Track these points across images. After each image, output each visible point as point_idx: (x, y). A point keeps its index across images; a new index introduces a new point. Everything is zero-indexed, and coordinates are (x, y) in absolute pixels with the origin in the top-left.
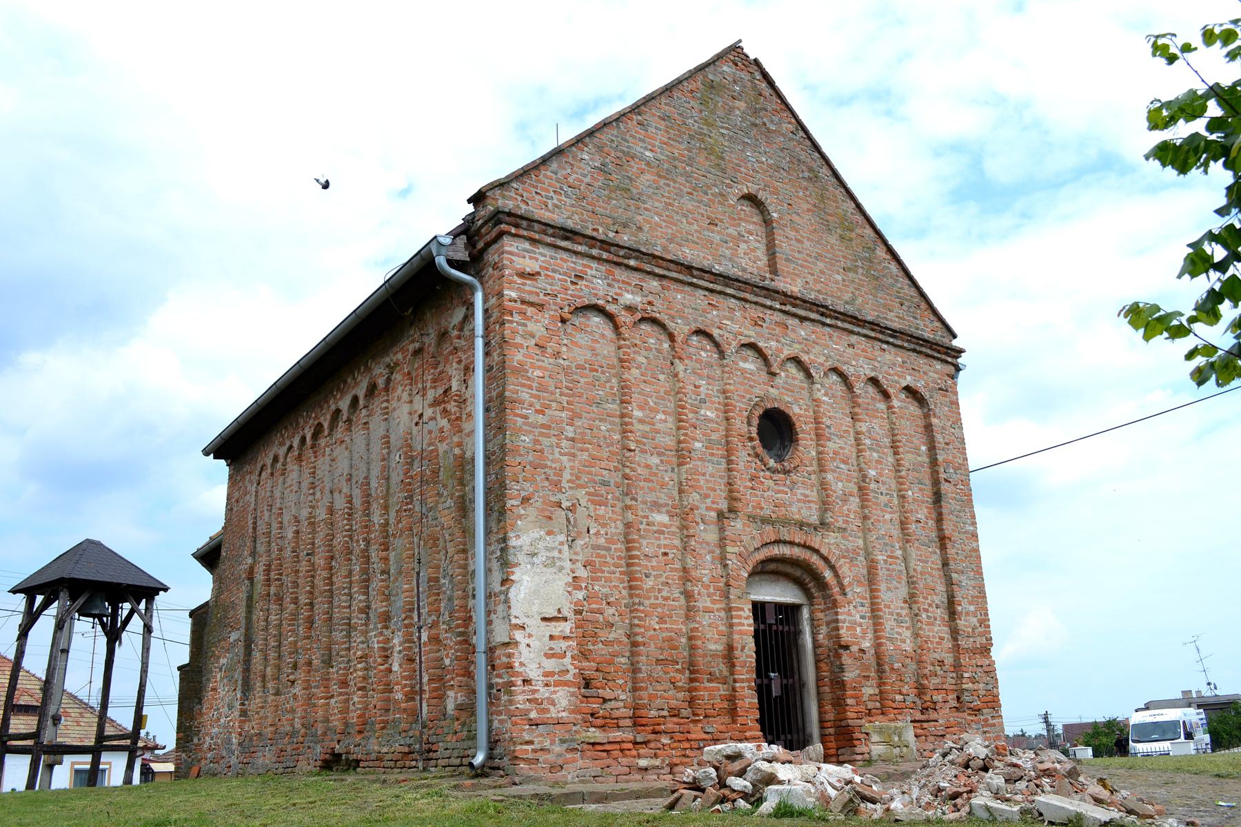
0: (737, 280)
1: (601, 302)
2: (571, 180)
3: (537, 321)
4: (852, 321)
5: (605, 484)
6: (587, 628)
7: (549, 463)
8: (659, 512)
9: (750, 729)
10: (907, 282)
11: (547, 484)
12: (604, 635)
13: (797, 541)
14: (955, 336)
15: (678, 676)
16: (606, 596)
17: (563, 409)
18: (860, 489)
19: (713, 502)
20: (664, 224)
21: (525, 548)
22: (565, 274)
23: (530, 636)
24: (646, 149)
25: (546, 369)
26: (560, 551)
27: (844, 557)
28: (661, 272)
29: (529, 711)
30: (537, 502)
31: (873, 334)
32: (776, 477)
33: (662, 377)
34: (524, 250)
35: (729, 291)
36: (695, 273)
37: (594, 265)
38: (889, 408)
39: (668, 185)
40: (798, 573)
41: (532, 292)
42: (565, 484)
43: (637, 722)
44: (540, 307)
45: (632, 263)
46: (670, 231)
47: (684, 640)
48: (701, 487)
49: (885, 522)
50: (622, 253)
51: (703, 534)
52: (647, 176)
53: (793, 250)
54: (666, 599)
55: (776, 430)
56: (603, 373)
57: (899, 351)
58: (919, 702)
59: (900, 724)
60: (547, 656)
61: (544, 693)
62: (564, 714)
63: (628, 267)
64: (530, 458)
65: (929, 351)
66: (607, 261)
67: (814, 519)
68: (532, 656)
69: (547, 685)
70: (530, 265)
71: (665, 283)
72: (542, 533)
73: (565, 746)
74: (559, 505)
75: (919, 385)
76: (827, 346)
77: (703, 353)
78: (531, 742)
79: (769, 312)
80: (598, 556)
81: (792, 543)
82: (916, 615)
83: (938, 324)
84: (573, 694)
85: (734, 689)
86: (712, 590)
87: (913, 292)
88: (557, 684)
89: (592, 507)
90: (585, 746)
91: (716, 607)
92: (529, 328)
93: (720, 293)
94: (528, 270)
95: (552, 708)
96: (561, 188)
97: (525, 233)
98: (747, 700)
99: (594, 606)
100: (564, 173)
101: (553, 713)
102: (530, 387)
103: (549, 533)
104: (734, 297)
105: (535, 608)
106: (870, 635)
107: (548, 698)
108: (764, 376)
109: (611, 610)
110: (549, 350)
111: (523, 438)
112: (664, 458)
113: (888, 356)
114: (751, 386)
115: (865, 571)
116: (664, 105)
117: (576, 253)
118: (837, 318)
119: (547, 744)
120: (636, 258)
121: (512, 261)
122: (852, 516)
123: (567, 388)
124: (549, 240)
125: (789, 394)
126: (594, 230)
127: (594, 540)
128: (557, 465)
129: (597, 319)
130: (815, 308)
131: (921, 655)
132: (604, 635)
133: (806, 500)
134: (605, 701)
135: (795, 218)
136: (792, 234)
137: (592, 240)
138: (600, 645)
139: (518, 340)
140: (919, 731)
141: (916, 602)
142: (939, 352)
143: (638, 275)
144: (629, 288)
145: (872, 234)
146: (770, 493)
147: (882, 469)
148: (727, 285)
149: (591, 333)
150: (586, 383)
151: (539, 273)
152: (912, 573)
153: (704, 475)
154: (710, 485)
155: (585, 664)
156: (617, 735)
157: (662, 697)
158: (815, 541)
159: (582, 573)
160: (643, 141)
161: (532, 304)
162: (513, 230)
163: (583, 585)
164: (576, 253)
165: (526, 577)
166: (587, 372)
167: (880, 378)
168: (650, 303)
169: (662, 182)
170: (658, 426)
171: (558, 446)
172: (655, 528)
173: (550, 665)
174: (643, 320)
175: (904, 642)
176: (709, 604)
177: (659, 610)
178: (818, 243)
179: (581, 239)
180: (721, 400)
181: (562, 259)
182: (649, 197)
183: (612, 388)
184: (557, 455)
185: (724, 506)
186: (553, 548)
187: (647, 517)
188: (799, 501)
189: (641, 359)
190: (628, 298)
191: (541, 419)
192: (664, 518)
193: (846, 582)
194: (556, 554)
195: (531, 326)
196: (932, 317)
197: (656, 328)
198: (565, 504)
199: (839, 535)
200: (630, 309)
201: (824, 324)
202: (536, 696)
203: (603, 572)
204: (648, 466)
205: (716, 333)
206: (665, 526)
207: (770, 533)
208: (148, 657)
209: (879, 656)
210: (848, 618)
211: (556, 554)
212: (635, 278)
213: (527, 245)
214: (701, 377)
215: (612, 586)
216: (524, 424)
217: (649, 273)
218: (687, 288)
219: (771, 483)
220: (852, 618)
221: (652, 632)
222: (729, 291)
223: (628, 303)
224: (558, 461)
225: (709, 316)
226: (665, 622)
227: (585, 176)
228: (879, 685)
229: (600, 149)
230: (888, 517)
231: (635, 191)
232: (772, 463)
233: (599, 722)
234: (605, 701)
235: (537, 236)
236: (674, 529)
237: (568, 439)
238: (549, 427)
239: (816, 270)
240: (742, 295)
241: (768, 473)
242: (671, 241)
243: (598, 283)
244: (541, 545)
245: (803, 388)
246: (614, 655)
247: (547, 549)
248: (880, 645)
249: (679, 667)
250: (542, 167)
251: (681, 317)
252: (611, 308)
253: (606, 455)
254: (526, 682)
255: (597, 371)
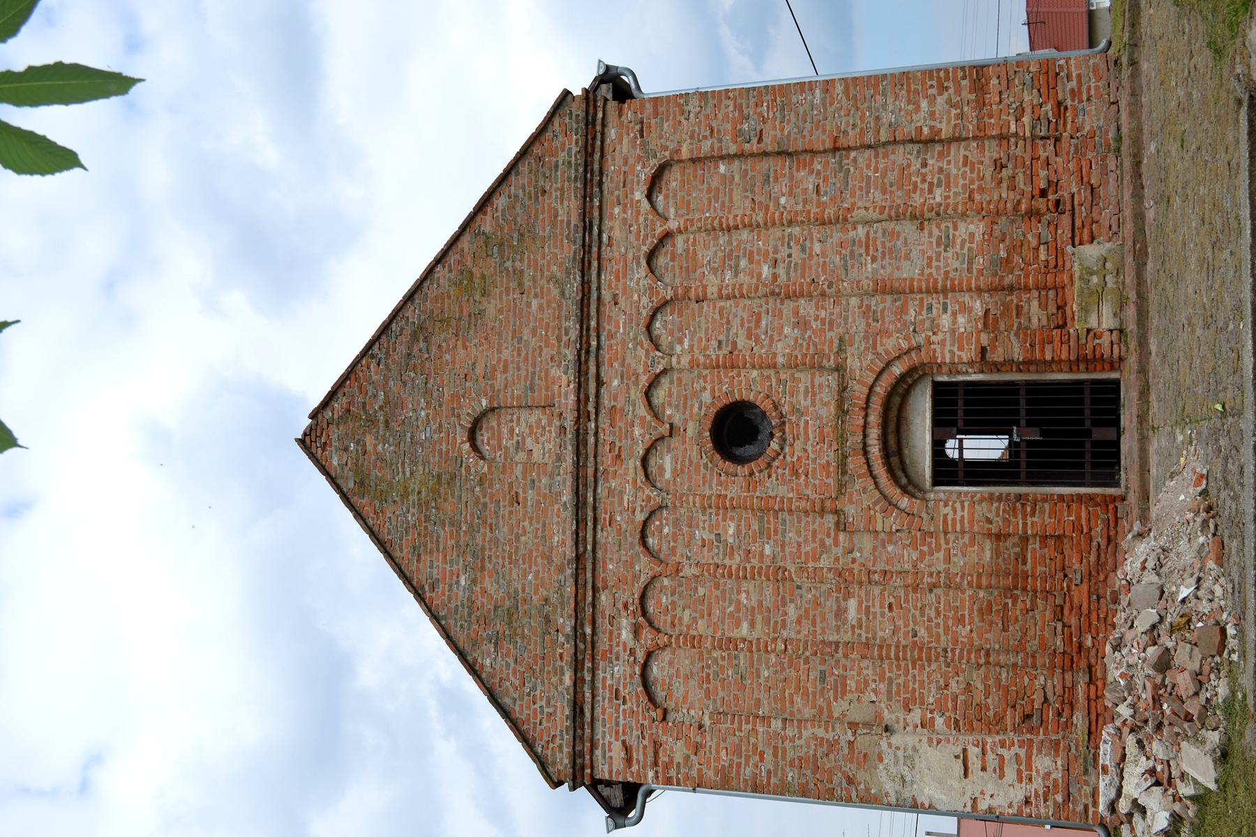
0: (577, 493)
1: (637, 670)
2: (517, 683)
3: (672, 751)
4: (587, 305)
5: (823, 678)
6: (972, 719)
7: (812, 752)
8: (846, 611)
9: (1079, 518)
10: (513, 177)
11: (832, 756)
12: (979, 697)
13: (861, 422)
14: (566, 94)
15: (1020, 605)
16: (939, 688)
17: (754, 730)
18: (788, 297)
19: (828, 536)
20: (534, 569)
21: (898, 788)
22: (617, 711)
23: (982, 793)
24: (458, 583)
25: (718, 745)
26: (898, 748)
27: (875, 347)
28: (590, 593)
29: (1055, 802)
30: (851, 768)
31: (595, 263)
32: (789, 438)
33: (701, 591)
34: (604, 757)
35: (590, 500)
36: (581, 549)
37: (600, 674)
38: (680, 232)
39: (490, 557)
41: (645, 754)
42: (830, 736)
43: (1069, 665)
44: (657, 745)
45: (588, 630)
46: (539, 560)
47: (982, 594)
48: (814, 550)
49: (824, 254)
50: (581, 646)
51: (866, 554)
53: (519, 377)
54: (938, 613)
55: (737, 431)
56: (709, 667)
57: (607, 210)
58: (1048, 217)
59: (1076, 268)
60: (1002, 776)
61: (1038, 784)
62: (1059, 763)
63: (594, 633)
64: (808, 772)
65: (597, 156)
66: (593, 659)
67: (832, 380)
68: (1002, 793)
69: (1030, 780)
70: (617, 752)
71: (600, 585)
72: (881, 767)
73: (1091, 769)
74: (851, 743)
75: (644, 174)
76: (624, 342)
77: (666, 530)
78: (1086, 807)
79: (601, 436)
80: (898, 693)
81: (865, 427)
82: (938, 214)
83: (556, 121)
85: (1034, 536)
86: (925, 548)
87: (524, 168)
88: (1029, 768)
89: (849, 696)
90: (1092, 744)
91: (943, 546)
92: (681, 761)
93: (595, 509)
94: (623, 755)
95: (1053, 776)
96: (529, 695)
97: (587, 757)
98: (1047, 520)
99: (950, 705)
100: (511, 690)
101: (1058, 775)
102: (739, 765)
103: (881, 759)
104: (595, 490)
105: (956, 785)
106: (966, 298)
107: (1044, 779)
108: (675, 442)
109: (953, 684)
110: (698, 739)
111: (790, 779)
112: (788, 598)
113: (617, 234)
114: (687, 460)
115: (889, 298)
116: (402, 554)
117: (593, 697)
118: (588, 329)
119: (1088, 789)
120: (582, 626)
121: (618, 773)
123: (732, 723)
124: (588, 731)
125: (693, 405)
126: (561, 658)
127: (883, 697)
129: (655, 669)
130: (583, 367)
131: (989, 212)
132: (979, 697)
133: (811, 392)
134: (1046, 700)
135: (479, 370)
136: (500, 377)
137: (577, 682)
138: (989, 701)
140: (1086, 237)
141: (922, 215)
144: (615, 633)
145: (466, 238)
146: (809, 449)
147: (759, 250)
148: (585, 503)
149: (671, 678)
150: (723, 689)
151: (624, 742)
152: (885, 216)
153: (799, 544)
154: (810, 537)
156: (1081, 690)
157: (1043, 629)
158: (860, 391)
159: (916, 716)
160: (451, 586)
161: (656, 753)
162: (588, 771)
163: (929, 716)
164: (593, 697)
165: (926, 791)
166: (711, 686)
167: (645, 249)
168: (626, 607)
169: (488, 566)
170: (754, 603)
172: (864, 618)
173: (1010, 774)
174: (644, 613)
175: (972, 235)
176: (941, 555)
177: (950, 623)
178: (500, 335)
179: (579, 696)
180: (713, 511)
181: (603, 714)
182: (509, 585)
183: (723, 658)
184: (802, 742)
185: (830, 520)
186: (895, 756)
187: (853, 627)
188: (813, 404)
190: (626, 635)
191: (768, 756)
192: (852, 604)
194: (900, 753)
195: (678, 758)
196: (549, 134)
197: (649, 594)
198: (850, 737)
199: (850, 350)
201: (599, 347)
202: (1041, 793)
203: (914, 689)
204: (799, 622)
205: (640, 517)
206: (860, 603)
207: (855, 463)
209: (992, 290)
210: (948, 347)
211: (900, 753)
213: (598, 752)
214: (692, 536)
216: (776, 776)
217: (594, 606)
218: (600, 555)
219: (798, 445)
220: (944, 354)
221: (974, 635)
222: (590, 500)
223: (631, 636)
224: (807, 741)
225: (624, 526)
226: (963, 616)
227: (508, 665)
228: (1027, 289)
229: (475, 644)
230: (817, 248)
231: (508, 603)
232: (774, 445)
233: (1067, 707)
234: (1046, 700)
235: (588, 744)
236: (863, 594)
237: (784, 728)
238: (776, 748)
239: (534, 342)
240: (591, 479)
241: (787, 449)
243: (617, 672)
244: (892, 769)
245: (680, 379)
246: (999, 686)
247: (896, 763)
249: (1010, 601)
250: (513, 716)
251: (632, 566)
252: (640, 656)
253: (793, 673)
254: (1027, 802)
255: (708, 675)
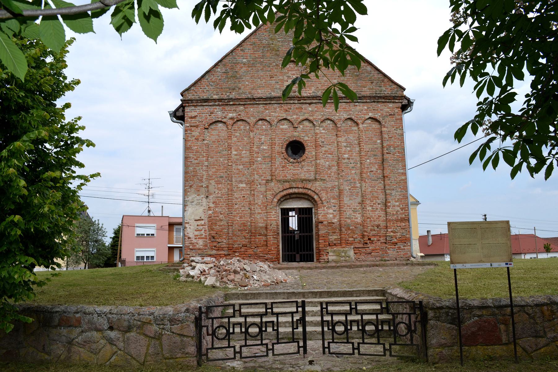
1: (220, 119)
5: (221, 177)
6: (212, 222)
9: (273, 251)
12: (218, 223)
14: (404, 89)
15: (246, 234)
16: (220, 212)
27: (323, 190)
28: (243, 103)
32: (294, 165)
33: (245, 139)
37: (218, 107)
40: (306, 197)
42: (204, 180)
43: (229, 249)
45: (231, 103)
50: (226, 101)
52: (244, 68)
54: (243, 211)
55: (296, 148)
59: (347, 249)
60: (196, 231)
61: (194, 241)
63: (230, 105)
65: (383, 100)
67: (312, 177)
70: (194, 114)
71: (246, 106)
74: (202, 186)
75: (377, 116)
77: (264, 127)
83: (395, 86)
84: (204, 241)
87: (380, 76)
88: (199, 238)
89: (216, 185)
93: (270, 104)
103: (198, 195)
105: (192, 217)
106: (338, 217)
113: (358, 108)
122: (333, 174)
124: (200, 104)
125: (303, 134)
127: (217, 195)
128: (201, 175)
132: (218, 223)
139: (189, 139)
142: (389, 99)
143: (234, 106)
148: (271, 100)
155: (212, 232)
158: (309, 186)
161: (194, 126)
168: (239, 115)
171: (202, 169)
173: (197, 233)
174: (238, 121)
176: (260, 211)
188: (305, 172)
189: (238, 134)
191: (196, 161)
192: (244, 185)
193: (323, 199)
194: (200, 201)
195: (193, 133)
196: (391, 84)
197: (244, 122)
199: (321, 183)
200: (232, 118)
204: (238, 169)
205: (268, 118)
206: (244, 188)
207: (287, 185)
208: (169, 238)
212: (234, 108)
213: (193, 108)
214: (262, 135)
215: (222, 209)
218: (255, 106)
220: (320, 211)
227: (218, 77)
228: (340, 235)
229: (224, 65)
232: (292, 160)
238: (199, 164)
241: (290, 164)
242: (252, 89)
243: (219, 113)
244: (195, 199)
247: (197, 200)
248: (340, 221)
251: (252, 116)
252: (224, 120)
253: (222, 168)
254: (189, 238)
